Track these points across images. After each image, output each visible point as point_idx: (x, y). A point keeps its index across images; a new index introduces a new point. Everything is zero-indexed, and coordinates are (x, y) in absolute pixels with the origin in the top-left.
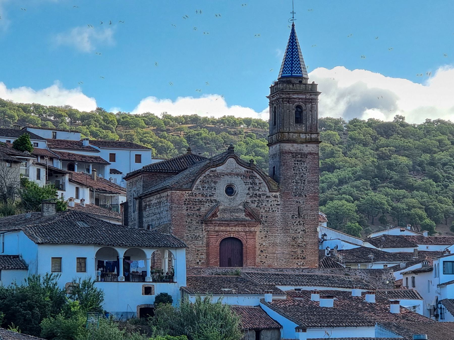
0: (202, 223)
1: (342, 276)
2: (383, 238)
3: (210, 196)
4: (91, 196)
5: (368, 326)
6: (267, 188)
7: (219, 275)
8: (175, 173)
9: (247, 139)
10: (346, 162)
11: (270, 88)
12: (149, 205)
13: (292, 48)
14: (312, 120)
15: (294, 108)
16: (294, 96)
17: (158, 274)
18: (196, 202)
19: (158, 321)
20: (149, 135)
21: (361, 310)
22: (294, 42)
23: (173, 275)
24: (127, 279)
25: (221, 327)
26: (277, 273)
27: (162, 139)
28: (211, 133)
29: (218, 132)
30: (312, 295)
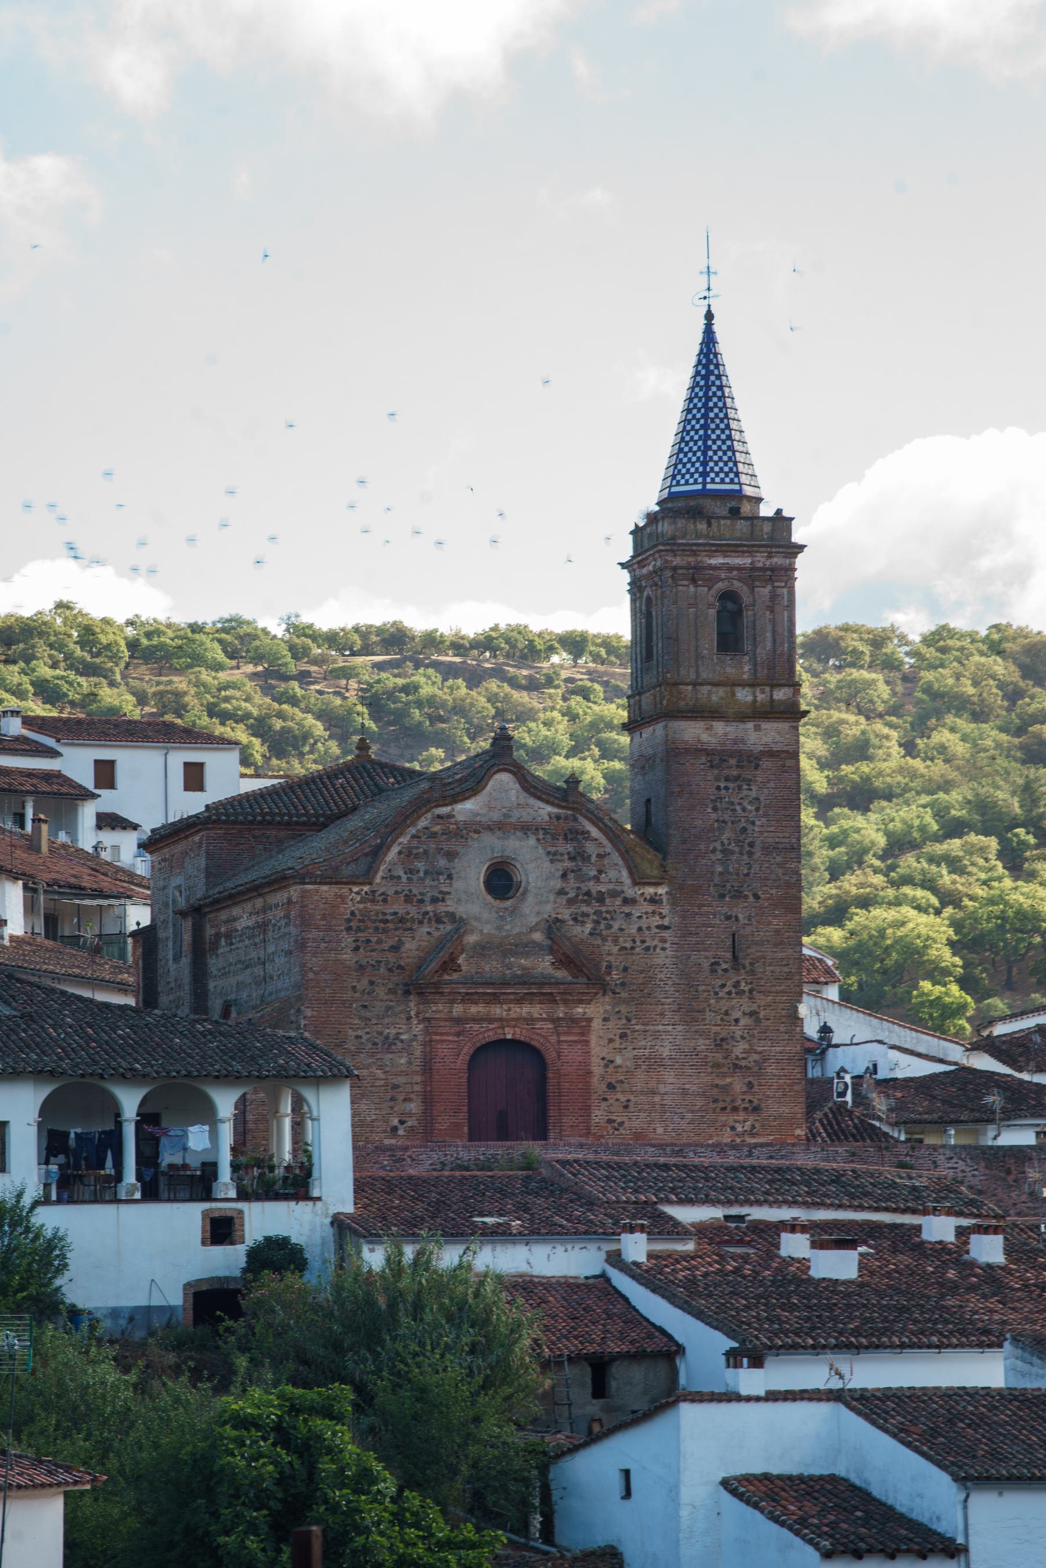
0: (407, 993)
1: (889, 1172)
2: (1037, 1038)
3: (434, 900)
4: (30, 908)
5: (981, 1345)
6: (625, 873)
7: (467, 1169)
8: (314, 824)
9: (573, 703)
10: (914, 775)
11: (632, 533)
12: (228, 936)
13: (706, 394)
14: (774, 641)
15: (711, 600)
16: (713, 561)
17: (256, 1172)
18: (387, 921)
19: (254, 1334)
20: (238, 694)
21: (953, 1288)
22: (712, 373)
23: (309, 1174)
24: (151, 1193)
25: (472, 1352)
26: (662, 1160)
27: (285, 706)
28: (450, 682)
29: (475, 678)
30: (786, 1238)
